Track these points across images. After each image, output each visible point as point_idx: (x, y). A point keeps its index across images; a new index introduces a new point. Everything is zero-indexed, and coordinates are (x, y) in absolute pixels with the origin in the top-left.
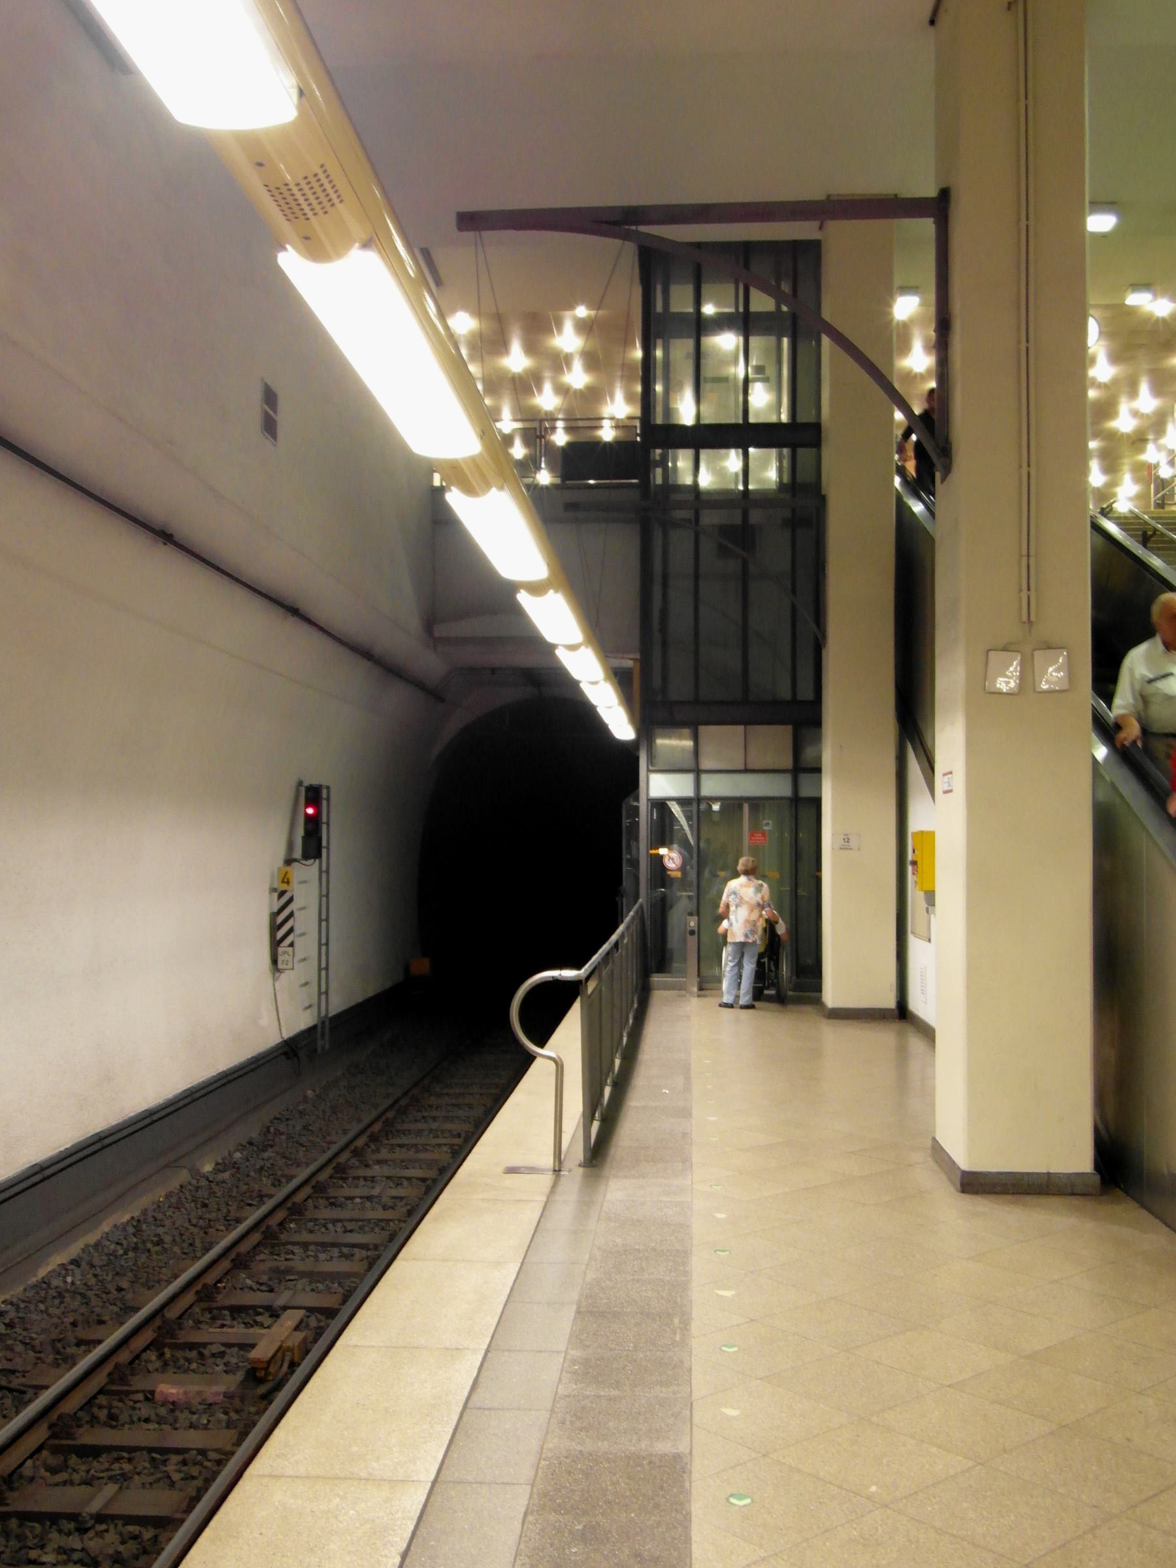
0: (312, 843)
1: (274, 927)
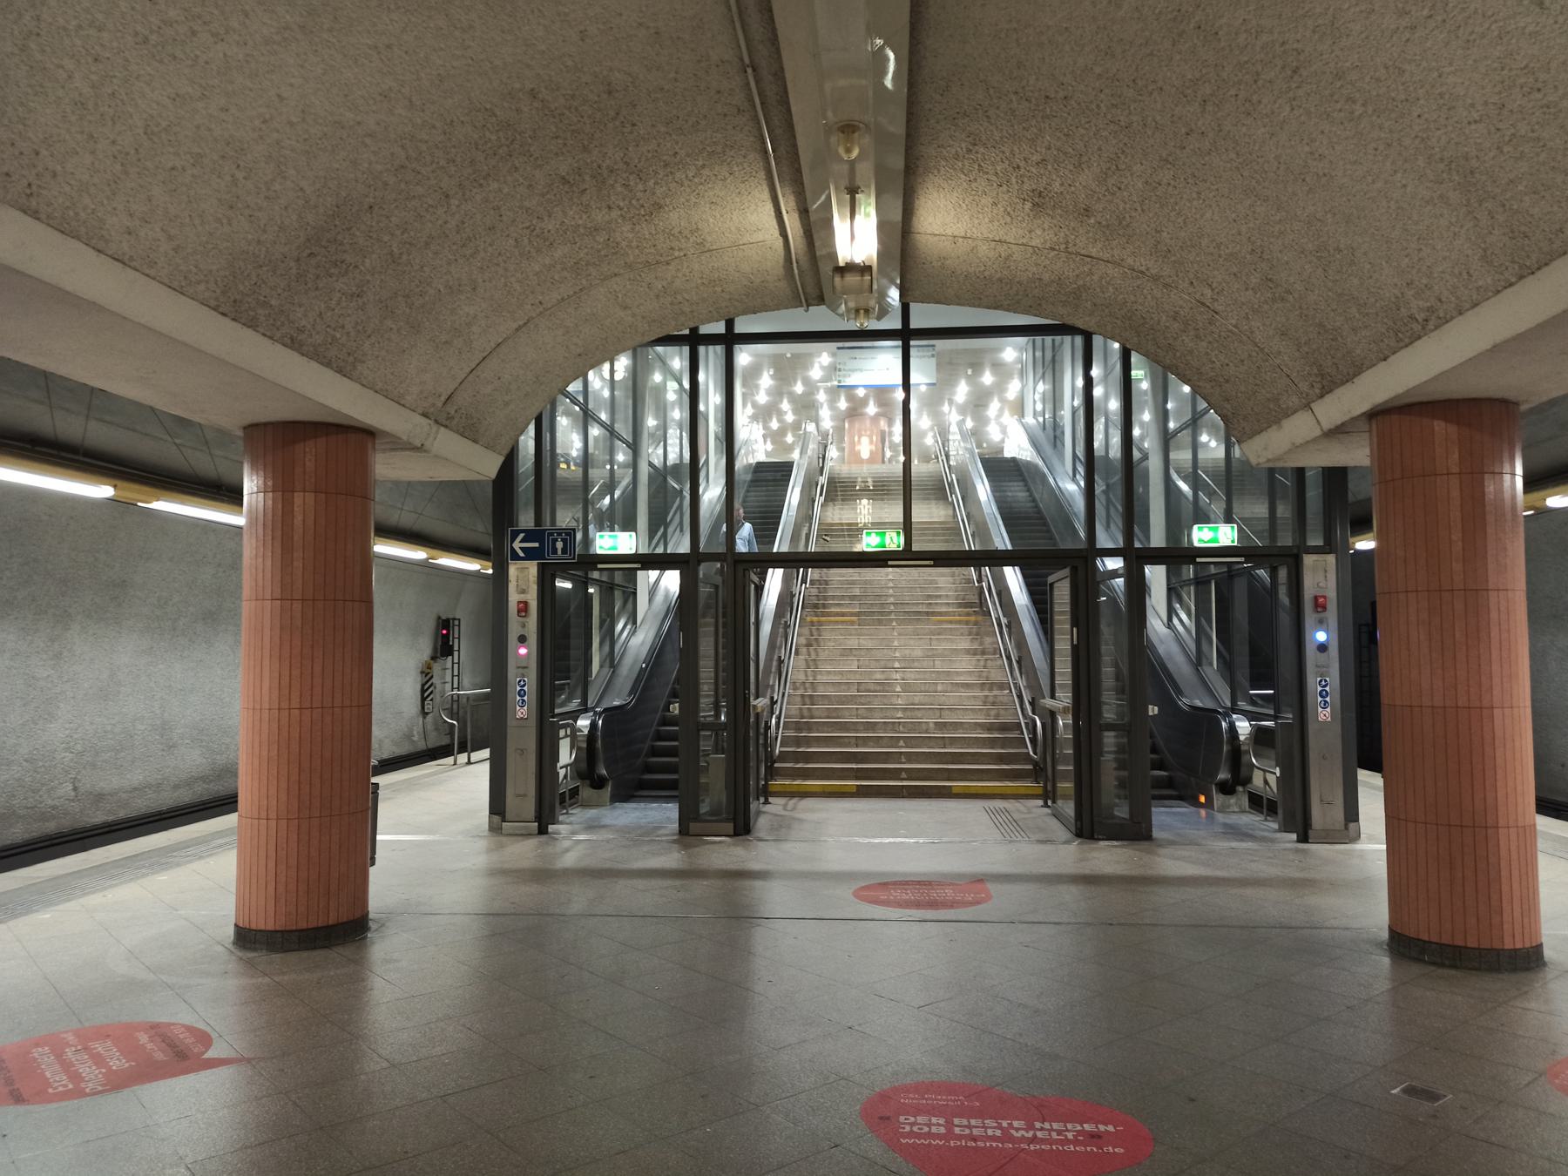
0: (444, 648)
1: (423, 691)
